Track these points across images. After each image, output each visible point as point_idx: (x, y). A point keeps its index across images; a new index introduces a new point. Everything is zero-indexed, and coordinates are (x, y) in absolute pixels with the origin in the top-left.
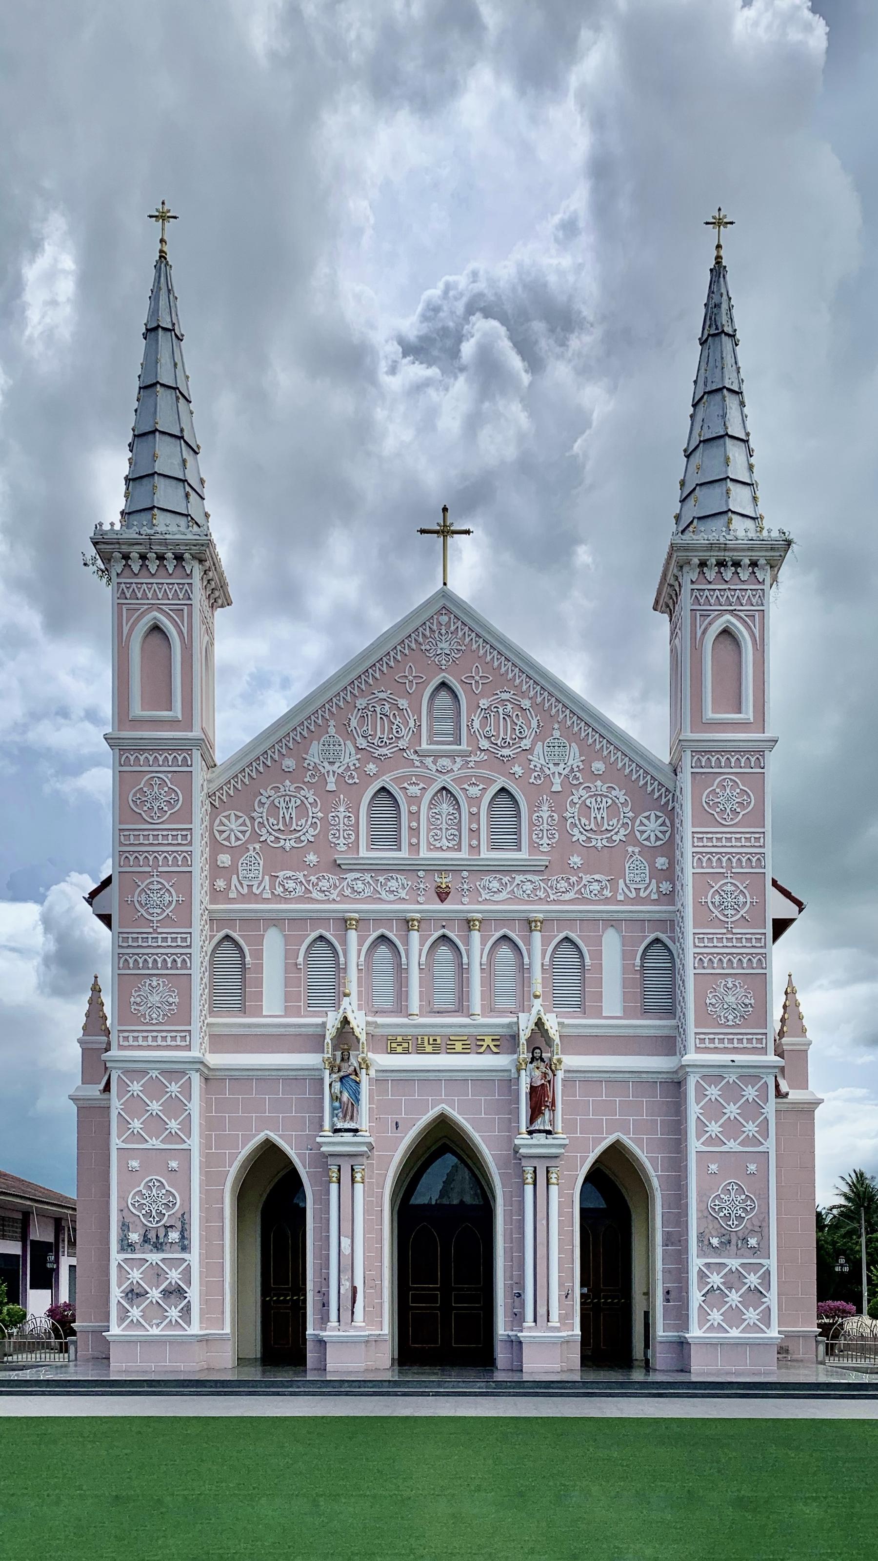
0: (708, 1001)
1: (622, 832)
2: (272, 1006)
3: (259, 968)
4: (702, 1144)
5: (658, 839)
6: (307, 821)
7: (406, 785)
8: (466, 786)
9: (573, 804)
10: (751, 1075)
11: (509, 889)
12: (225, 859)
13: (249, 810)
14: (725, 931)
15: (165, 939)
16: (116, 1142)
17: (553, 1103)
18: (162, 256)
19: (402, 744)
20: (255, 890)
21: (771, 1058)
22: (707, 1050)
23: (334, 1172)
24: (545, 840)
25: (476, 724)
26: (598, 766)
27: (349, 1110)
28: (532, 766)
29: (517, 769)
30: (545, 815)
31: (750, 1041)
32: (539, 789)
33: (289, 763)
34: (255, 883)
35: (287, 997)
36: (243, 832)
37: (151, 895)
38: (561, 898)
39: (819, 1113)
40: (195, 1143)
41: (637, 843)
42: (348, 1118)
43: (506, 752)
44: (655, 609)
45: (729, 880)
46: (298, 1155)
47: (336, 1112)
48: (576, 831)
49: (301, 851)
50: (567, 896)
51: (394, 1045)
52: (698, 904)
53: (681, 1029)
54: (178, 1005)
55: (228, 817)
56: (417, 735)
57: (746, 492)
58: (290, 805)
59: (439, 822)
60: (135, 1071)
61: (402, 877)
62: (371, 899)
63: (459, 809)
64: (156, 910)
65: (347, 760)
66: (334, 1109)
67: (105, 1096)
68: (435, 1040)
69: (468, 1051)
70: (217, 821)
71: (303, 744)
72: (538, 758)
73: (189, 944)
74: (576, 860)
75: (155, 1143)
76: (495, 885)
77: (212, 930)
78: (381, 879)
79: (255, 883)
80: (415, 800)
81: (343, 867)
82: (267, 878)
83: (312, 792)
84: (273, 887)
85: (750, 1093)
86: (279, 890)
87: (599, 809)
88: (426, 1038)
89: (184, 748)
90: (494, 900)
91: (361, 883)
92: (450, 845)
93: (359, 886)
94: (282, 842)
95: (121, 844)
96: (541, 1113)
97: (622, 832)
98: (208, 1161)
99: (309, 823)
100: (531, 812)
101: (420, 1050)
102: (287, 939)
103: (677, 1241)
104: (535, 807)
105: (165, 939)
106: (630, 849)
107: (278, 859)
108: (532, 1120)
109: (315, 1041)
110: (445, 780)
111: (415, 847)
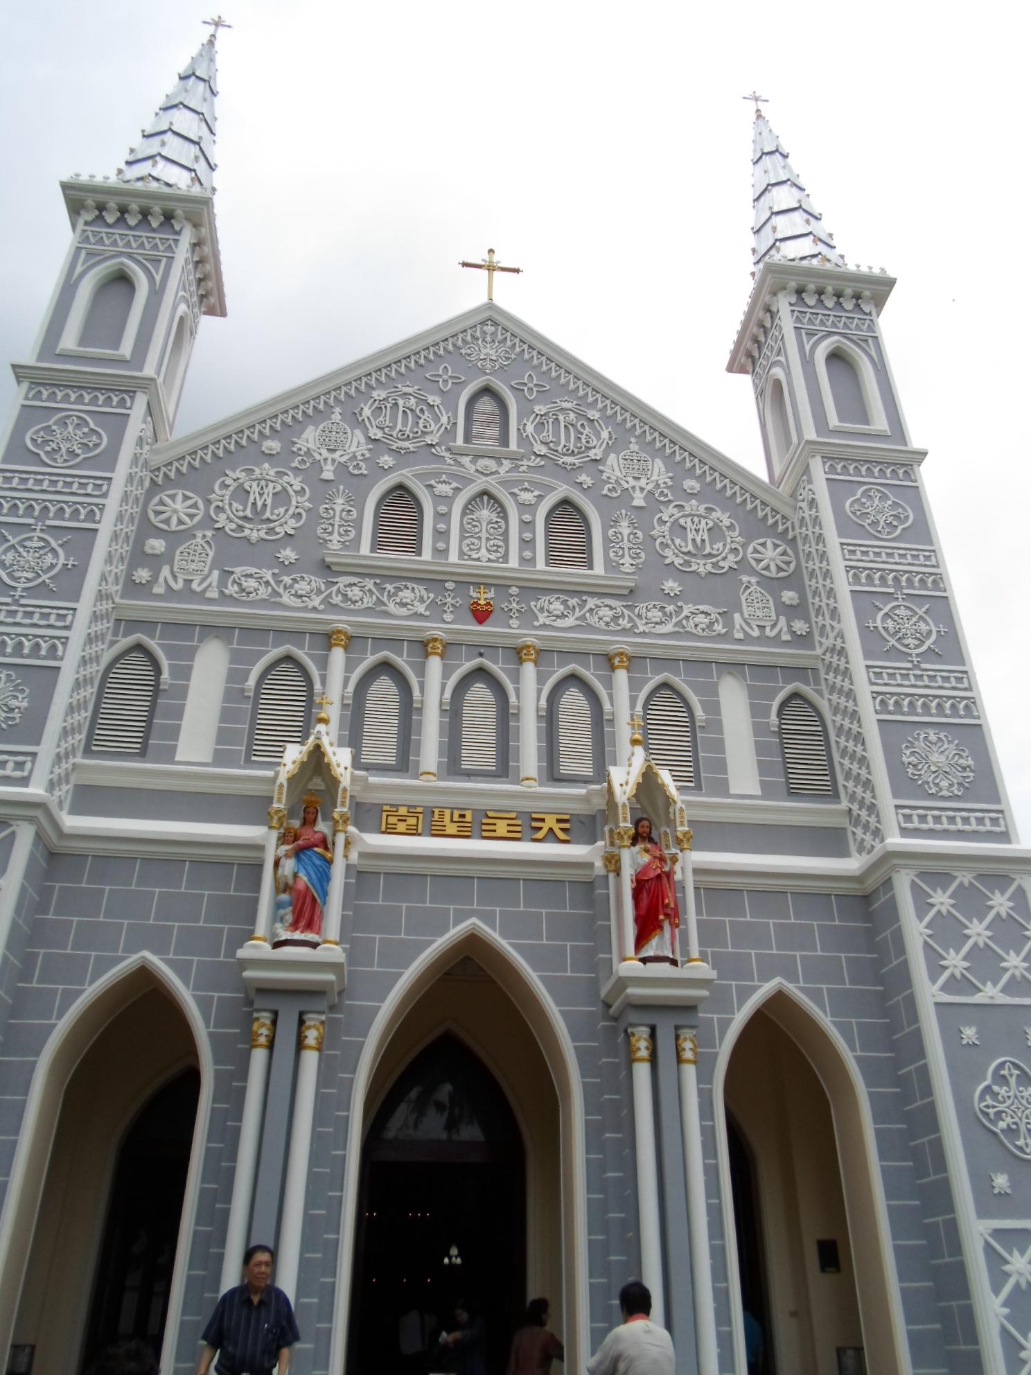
0: (905, 759)
2: (196, 741)
3: (183, 692)
4: (943, 989)
6: (287, 510)
7: (433, 482)
8: (516, 491)
9: (662, 522)
11: (577, 614)
12: (157, 545)
14: (910, 665)
15: (29, 615)
20: (194, 586)
22: (916, 833)
23: (264, 1025)
25: (530, 428)
26: (691, 484)
27: (305, 910)
28: (604, 477)
29: (584, 478)
30: (626, 532)
32: (614, 502)
33: (273, 445)
35: (223, 736)
37: (25, 554)
38: (654, 631)
41: (754, 572)
42: (302, 924)
45: (900, 602)
47: (282, 912)
48: (668, 553)
51: (392, 820)
54: (25, 713)
55: (173, 497)
56: (450, 432)
58: (266, 491)
59: (477, 530)
61: (421, 588)
62: (368, 611)
64: (25, 574)
65: (353, 449)
66: (278, 905)
68: (463, 816)
69: (518, 835)
70: (156, 500)
73: (68, 623)
74: (671, 585)
76: (557, 607)
77: (116, 634)
78: (389, 587)
80: (448, 500)
81: (334, 568)
82: (216, 573)
83: (299, 479)
84: (222, 583)
86: (232, 589)
87: (697, 531)
88: (447, 812)
90: (555, 621)
91: (360, 592)
92: (492, 557)
93: (355, 593)
94: (247, 532)
97: (731, 557)
99: (290, 512)
102: (752, 693)
104: (610, 522)
105: (29, 615)
106: (745, 579)
108: (641, 941)
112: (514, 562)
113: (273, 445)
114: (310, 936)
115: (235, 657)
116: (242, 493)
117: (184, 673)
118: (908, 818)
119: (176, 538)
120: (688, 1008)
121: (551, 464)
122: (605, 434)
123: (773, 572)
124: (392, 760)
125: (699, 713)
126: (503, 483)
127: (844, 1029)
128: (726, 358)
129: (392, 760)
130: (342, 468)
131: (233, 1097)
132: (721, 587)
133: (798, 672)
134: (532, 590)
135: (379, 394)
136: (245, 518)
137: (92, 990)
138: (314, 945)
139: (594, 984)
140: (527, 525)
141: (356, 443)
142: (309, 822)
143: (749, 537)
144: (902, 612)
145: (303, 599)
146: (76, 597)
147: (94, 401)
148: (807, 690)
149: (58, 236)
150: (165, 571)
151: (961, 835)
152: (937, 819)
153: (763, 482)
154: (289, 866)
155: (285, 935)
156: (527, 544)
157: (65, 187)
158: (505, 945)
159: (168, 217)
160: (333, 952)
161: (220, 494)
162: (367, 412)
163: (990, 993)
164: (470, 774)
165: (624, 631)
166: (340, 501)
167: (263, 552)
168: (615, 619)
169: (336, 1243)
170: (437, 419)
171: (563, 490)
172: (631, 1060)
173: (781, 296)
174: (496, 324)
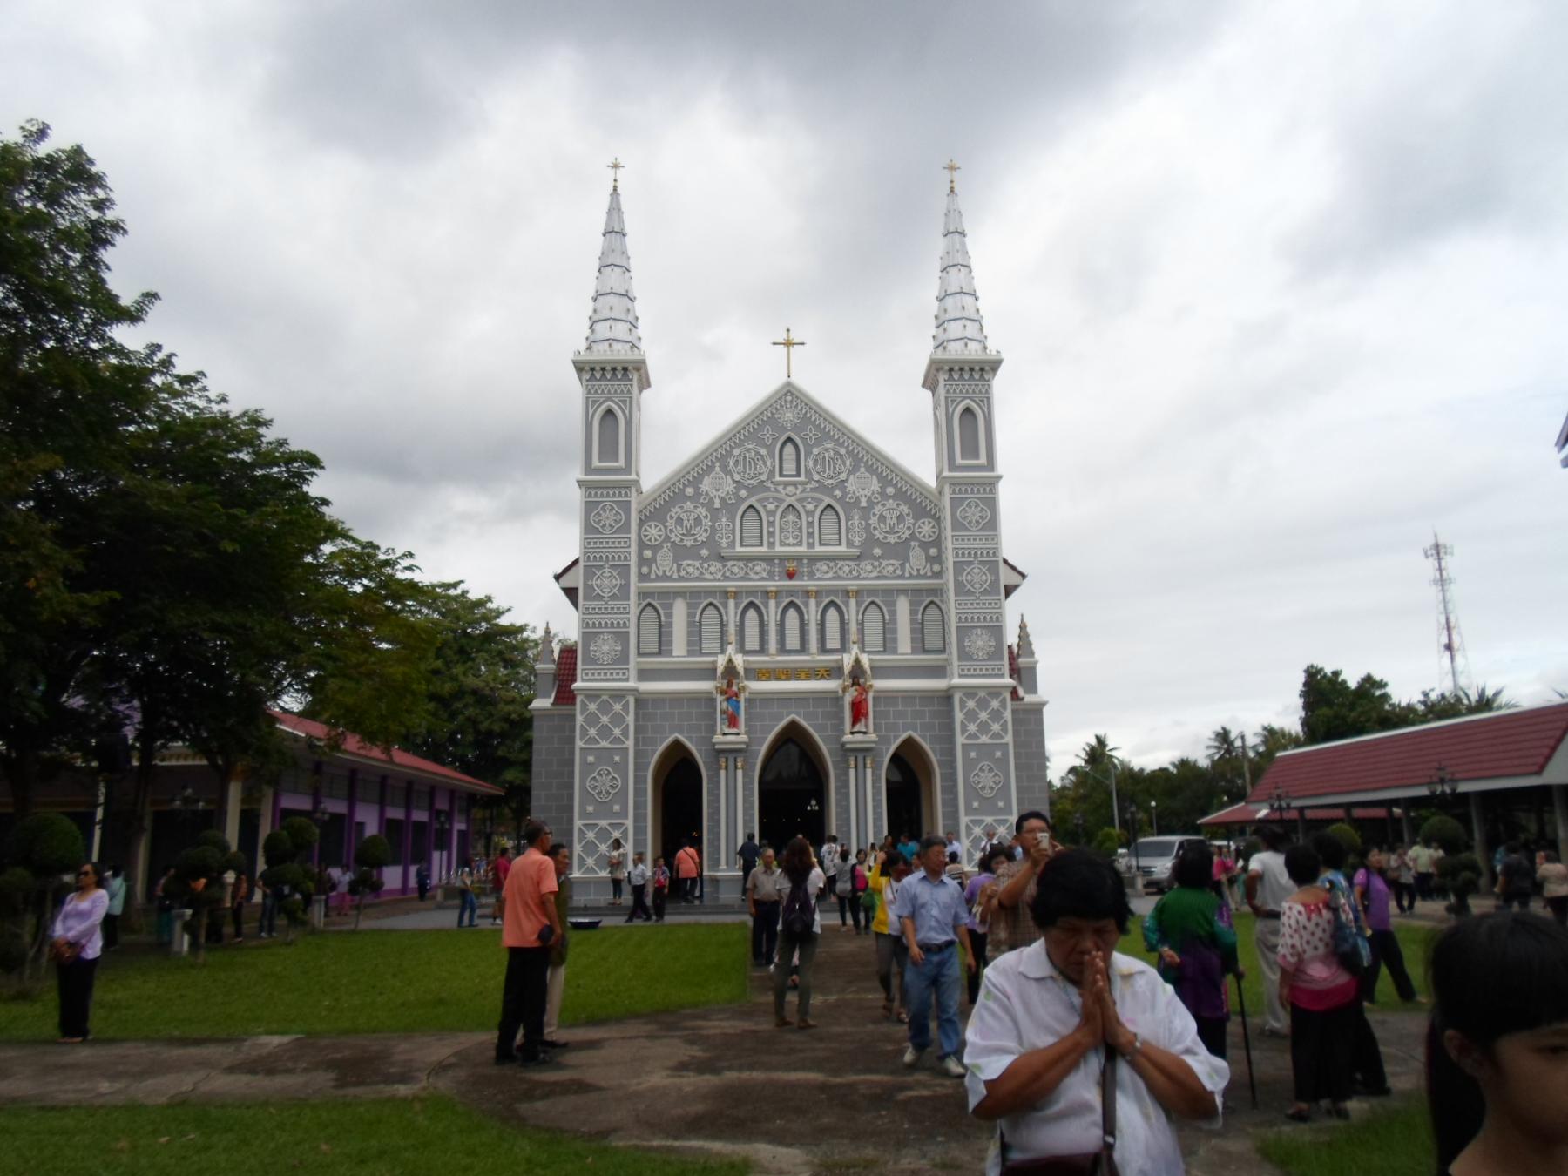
2: (679, 651)
3: (670, 625)
10: (994, 692)
12: (648, 553)
13: (663, 521)
16: (579, 744)
18: (615, 188)
19: (763, 478)
21: (1008, 681)
27: (733, 721)
29: (838, 493)
32: (851, 505)
35: (690, 643)
39: (1046, 710)
40: (630, 744)
56: (772, 472)
57: (977, 325)
60: (593, 695)
62: (742, 579)
67: (564, 709)
71: (696, 482)
72: (850, 487)
74: (877, 551)
75: (604, 744)
76: (825, 568)
85: (995, 704)
86: (683, 573)
89: (627, 486)
90: (823, 578)
93: (735, 570)
98: (637, 754)
101: (778, 679)
102: (912, 604)
103: (952, 804)
109: (708, 673)
110: (792, 500)
111: (771, 545)
115: (689, 606)
116: (679, 521)
117: (669, 615)
121: (823, 488)
130: (723, 500)
132: (899, 551)
134: (813, 560)
140: (810, 524)
141: (729, 486)
142: (730, 685)
149: (574, 388)
151: (984, 676)
154: (725, 705)
156: (810, 535)
157: (575, 363)
161: (670, 523)
163: (984, 739)
164: (790, 652)
165: (855, 578)
167: (692, 553)
171: (827, 500)
172: (848, 767)
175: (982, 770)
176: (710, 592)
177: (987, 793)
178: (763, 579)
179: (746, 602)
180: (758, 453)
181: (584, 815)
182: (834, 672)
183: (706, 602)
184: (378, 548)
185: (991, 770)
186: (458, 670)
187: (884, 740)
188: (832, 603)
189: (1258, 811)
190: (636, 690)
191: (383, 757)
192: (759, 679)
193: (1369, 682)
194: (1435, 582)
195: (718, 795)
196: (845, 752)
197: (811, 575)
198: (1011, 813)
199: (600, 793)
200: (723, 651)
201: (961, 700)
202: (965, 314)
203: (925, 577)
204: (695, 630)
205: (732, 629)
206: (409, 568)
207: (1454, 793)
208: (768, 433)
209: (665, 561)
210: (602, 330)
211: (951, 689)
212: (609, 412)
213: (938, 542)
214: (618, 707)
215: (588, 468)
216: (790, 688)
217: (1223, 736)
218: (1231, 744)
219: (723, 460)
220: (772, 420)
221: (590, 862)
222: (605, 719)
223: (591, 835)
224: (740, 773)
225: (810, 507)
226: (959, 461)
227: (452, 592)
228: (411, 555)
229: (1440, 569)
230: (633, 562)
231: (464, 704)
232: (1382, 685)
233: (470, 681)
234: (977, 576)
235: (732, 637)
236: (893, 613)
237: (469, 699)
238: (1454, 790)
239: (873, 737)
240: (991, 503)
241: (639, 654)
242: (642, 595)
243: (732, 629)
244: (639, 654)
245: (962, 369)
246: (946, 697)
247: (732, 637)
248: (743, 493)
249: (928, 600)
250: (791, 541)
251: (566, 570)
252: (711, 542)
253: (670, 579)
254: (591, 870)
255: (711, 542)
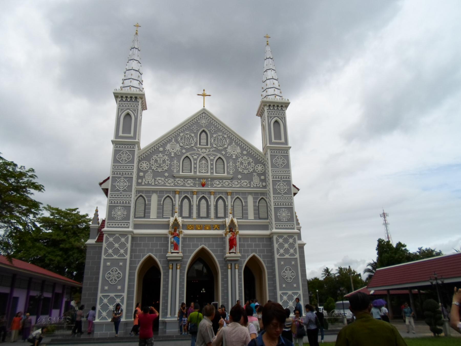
1: (252, 169)
2: (153, 216)
3: (150, 205)
5: (261, 171)
9: (238, 162)
12: (141, 174)
13: (149, 161)
15: (124, 196)
16: (103, 257)
17: (236, 244)
19: (193, 145)
24: (231, 171)
25: (212, 141)
29: (223, 152)
31: (290, 226)
32: (229, 158)
34: (150, 181)
35: (158, 213)
36: (147, 167)
39: (305, 247)
40: (128, 257)
41: (256, 172)
43: (220, 148)
44: (257, 115)
46: (263, 261)
49: (163, 172)
50: (237, 186)
52: (273, 188)
53: (271, 223)
55: (143, 163)
56: (196, 143)
60: (111, 234)
62: (182, 186)
63: (208, 162)
66: (171, 246)
71: (164, 145)
74: (240, 176)
75: (115, 257)
76: (218, 183)
78: (186, 180)
79: (150, 181)
80: (196, 160)
84: (155, 182)
86: (157, 183)
90: (217, 186)
91: (180, 182)
93: (179, 182)
95: (113, 169)
96: (233, 247)
100: (227, 164)
102: (254, 198)
107: (156, 174)
108: (230, 249)
109: (166, 226)
110: (204, 155)
111: (195, 172)
112: (209, 174)
113: (161, 149)
114: (177, 251)
115: (159, 197)
116: (156, 161)
117: (150, 201)
118: (277, 226)
119: (145, 172)
120: (237, 261)
122: (228, 141)
123: (260, 172)
124: (188, 216)
125: (244, 204)
126: (207, 155)
127: (264, 261)
128: (256, 113)
129: (188, 216)
130: (175, 153)
131: (167, 276)
132: (249, 177)
133: (263, 194)
134: (213, 179)
135: (181, 134)
136: (157, 167)
137: (142, 260)
138: (178, 253)
139: (223, 255)
140: (212, 164)
141: (178, 148)
142: (175, 231)
143: (256, 164)
144: (282, 184)
145: (170, 185)
146: (131, 192)
147: (128, 147)
148: (264, 197)
150: (144, 180)
152: (282, 226)
153: (260, 152)
154: (173, 239)
155: (173, 251)
156: (212, 169)
157: (114, 93)
158: (208, 249)
159: (136, 98)
160: (181, 254)
162: (179, 139)
163: (287, 256)
165: (230, 187)
166: (175, 161)
167: (161, 174)
168: (229, 184)
169: (183, 297)
170: (193, 140)
171: (219, 155)
172: (228, 269)
173: (265, 107)
174: (205, 114)
175: (286, 270)
176: (168, 191)
177: (289, 280)
178: (191, 186)
179: (184, 196)
180: (191, 135)
181: (103, 291)
182: (222, 226)
183: (166, 195)
184: (16, 165)
185: (290, 270)
186: (72, 240)
187: (243, 257)
188: (221, 197)
189: (370, 291)
190: (132, 232)
191: (8, 263)
192: (188, 229)
193: (400, 245)
194: (384, 224)
195: (168, 294)
196: (226, 262)
197: (212, 185)
198: (299, 290)
199: (111, 280)
200: (173, 216)
201: (277, 239)
202: (274, 86)
203: (259, 187)
204: (161, 208)
205: (177, 207)
206: (31, 176)
207: (443, 284)
208: (195, 127)
209: (149, 178)
210: (127, 83)
211: (272, 234)
212: (128, 114)
213: (264, 174)
214: (123, 240)
215: (117, 135)
216: (201, 232)
217: (327, 271)
218: (329, 273)
219: (176, 137)
220: (197, 123)
221: (104, 314)
222: (117, 245)
223: (105, 301)
224: (178, 271)
225: (212, 158)
226: (273, 140)
227: (74, 212)
228: (33, 170)
229: (385, 220)
230: (135, 176)
231: (66, 246)
232: (404, 246)
233: (77, 244)
234: (282, 186)
235: (177, 210)
236: (246, 202)
237: (76, 251)
238: (442, 282)
239: (239, 255)
240: (287, 157)
241: (135, 217)
242: (138, 191)
243: (177, 207)
244: (135, 217)
245: (274, 106)
246: (269, 238)
247: (177, 210)
248: (184, 151)
249: (261, 198)
250: (203, 171)
251: (105, 181)
252: (169, 170)
253: (151, 185)
254: (105, 318)
255: (169, 170)
